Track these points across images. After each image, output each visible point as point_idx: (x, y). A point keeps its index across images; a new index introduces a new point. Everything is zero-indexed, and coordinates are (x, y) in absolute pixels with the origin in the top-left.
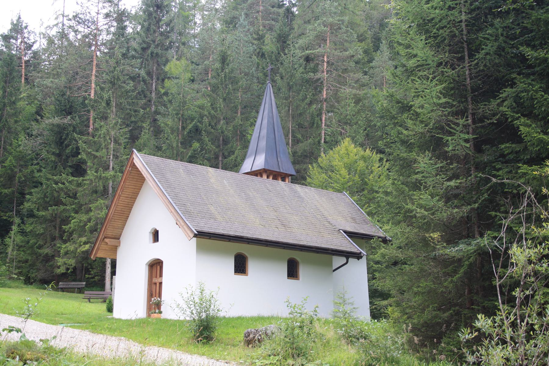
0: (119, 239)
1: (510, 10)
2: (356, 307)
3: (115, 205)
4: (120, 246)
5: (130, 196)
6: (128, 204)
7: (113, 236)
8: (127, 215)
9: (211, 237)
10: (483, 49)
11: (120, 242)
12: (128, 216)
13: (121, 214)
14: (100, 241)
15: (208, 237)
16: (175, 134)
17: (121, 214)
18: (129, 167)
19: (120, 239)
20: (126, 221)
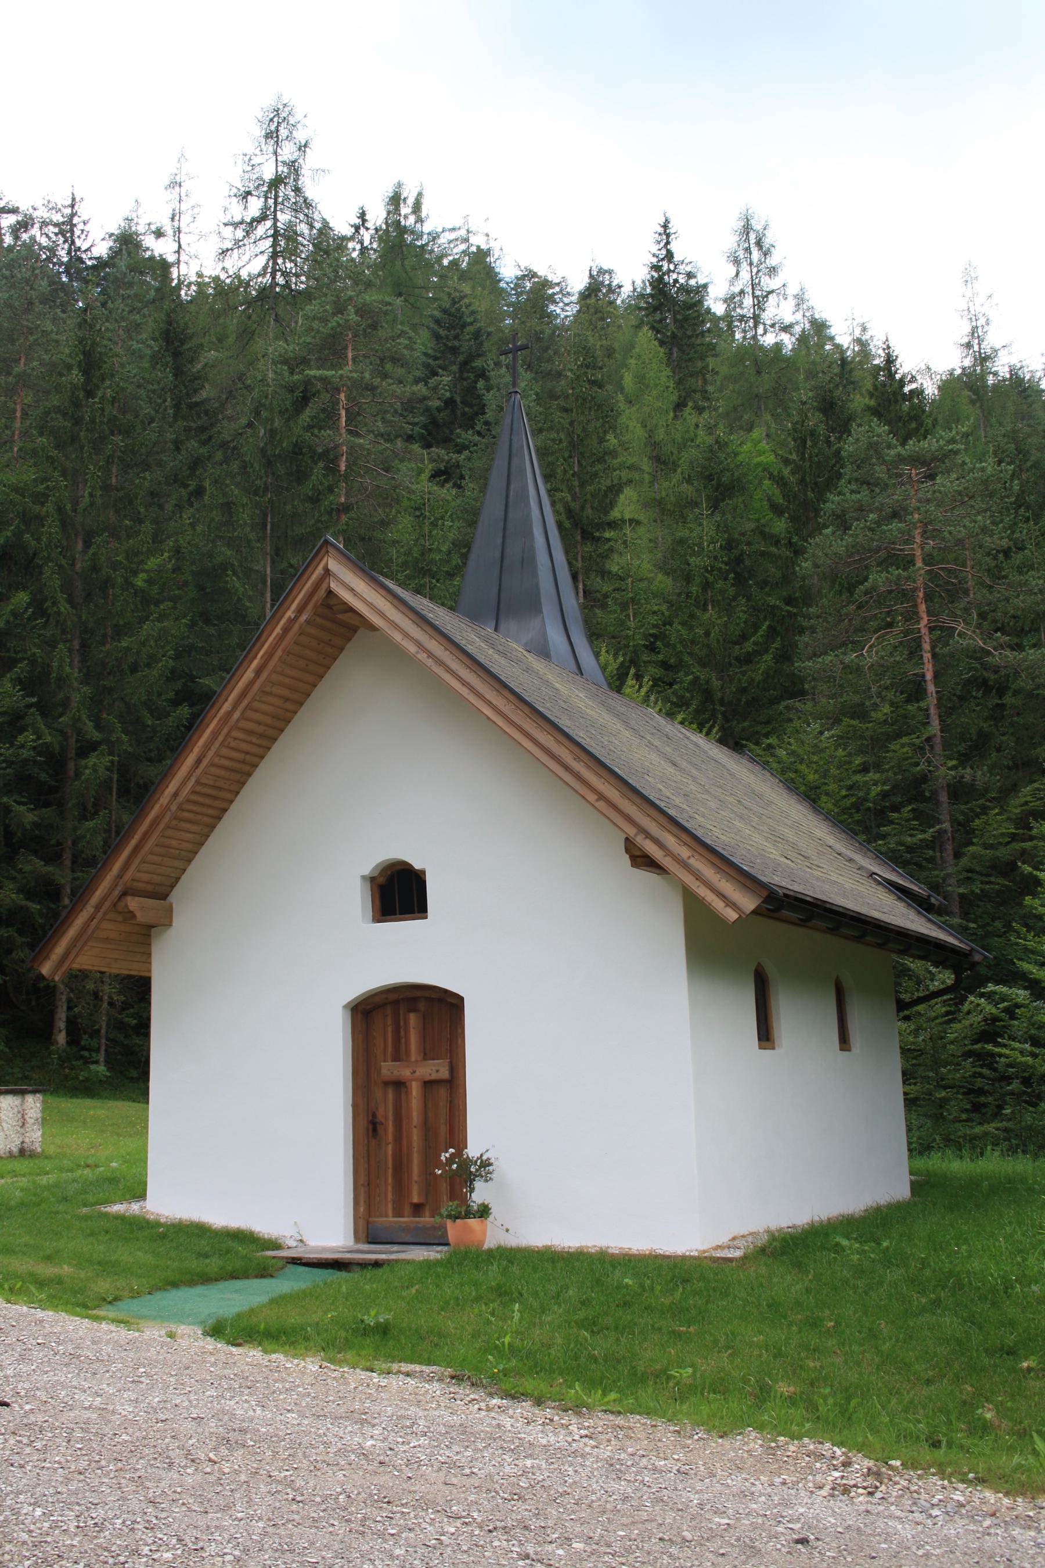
0: (164, 897)
1: (1034, 520)
2: (260, 256)
3: (199, 761)
4: (170, 925)
5: (261, 729)
6: (243, 762)
7: (150, 888)
8: (224, 805)
9: (808, 919)
10: (762, 636)
11: (170, 911)
12: (225, 810)
13: (207, 801)
14: (98, 907)
15: (794, 916)
16: (478, 363)
17: (207, 801)
18: (300, 610)
19: (174, 897)
20: (213, 827)
